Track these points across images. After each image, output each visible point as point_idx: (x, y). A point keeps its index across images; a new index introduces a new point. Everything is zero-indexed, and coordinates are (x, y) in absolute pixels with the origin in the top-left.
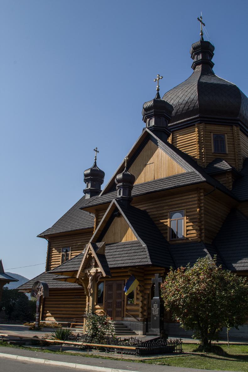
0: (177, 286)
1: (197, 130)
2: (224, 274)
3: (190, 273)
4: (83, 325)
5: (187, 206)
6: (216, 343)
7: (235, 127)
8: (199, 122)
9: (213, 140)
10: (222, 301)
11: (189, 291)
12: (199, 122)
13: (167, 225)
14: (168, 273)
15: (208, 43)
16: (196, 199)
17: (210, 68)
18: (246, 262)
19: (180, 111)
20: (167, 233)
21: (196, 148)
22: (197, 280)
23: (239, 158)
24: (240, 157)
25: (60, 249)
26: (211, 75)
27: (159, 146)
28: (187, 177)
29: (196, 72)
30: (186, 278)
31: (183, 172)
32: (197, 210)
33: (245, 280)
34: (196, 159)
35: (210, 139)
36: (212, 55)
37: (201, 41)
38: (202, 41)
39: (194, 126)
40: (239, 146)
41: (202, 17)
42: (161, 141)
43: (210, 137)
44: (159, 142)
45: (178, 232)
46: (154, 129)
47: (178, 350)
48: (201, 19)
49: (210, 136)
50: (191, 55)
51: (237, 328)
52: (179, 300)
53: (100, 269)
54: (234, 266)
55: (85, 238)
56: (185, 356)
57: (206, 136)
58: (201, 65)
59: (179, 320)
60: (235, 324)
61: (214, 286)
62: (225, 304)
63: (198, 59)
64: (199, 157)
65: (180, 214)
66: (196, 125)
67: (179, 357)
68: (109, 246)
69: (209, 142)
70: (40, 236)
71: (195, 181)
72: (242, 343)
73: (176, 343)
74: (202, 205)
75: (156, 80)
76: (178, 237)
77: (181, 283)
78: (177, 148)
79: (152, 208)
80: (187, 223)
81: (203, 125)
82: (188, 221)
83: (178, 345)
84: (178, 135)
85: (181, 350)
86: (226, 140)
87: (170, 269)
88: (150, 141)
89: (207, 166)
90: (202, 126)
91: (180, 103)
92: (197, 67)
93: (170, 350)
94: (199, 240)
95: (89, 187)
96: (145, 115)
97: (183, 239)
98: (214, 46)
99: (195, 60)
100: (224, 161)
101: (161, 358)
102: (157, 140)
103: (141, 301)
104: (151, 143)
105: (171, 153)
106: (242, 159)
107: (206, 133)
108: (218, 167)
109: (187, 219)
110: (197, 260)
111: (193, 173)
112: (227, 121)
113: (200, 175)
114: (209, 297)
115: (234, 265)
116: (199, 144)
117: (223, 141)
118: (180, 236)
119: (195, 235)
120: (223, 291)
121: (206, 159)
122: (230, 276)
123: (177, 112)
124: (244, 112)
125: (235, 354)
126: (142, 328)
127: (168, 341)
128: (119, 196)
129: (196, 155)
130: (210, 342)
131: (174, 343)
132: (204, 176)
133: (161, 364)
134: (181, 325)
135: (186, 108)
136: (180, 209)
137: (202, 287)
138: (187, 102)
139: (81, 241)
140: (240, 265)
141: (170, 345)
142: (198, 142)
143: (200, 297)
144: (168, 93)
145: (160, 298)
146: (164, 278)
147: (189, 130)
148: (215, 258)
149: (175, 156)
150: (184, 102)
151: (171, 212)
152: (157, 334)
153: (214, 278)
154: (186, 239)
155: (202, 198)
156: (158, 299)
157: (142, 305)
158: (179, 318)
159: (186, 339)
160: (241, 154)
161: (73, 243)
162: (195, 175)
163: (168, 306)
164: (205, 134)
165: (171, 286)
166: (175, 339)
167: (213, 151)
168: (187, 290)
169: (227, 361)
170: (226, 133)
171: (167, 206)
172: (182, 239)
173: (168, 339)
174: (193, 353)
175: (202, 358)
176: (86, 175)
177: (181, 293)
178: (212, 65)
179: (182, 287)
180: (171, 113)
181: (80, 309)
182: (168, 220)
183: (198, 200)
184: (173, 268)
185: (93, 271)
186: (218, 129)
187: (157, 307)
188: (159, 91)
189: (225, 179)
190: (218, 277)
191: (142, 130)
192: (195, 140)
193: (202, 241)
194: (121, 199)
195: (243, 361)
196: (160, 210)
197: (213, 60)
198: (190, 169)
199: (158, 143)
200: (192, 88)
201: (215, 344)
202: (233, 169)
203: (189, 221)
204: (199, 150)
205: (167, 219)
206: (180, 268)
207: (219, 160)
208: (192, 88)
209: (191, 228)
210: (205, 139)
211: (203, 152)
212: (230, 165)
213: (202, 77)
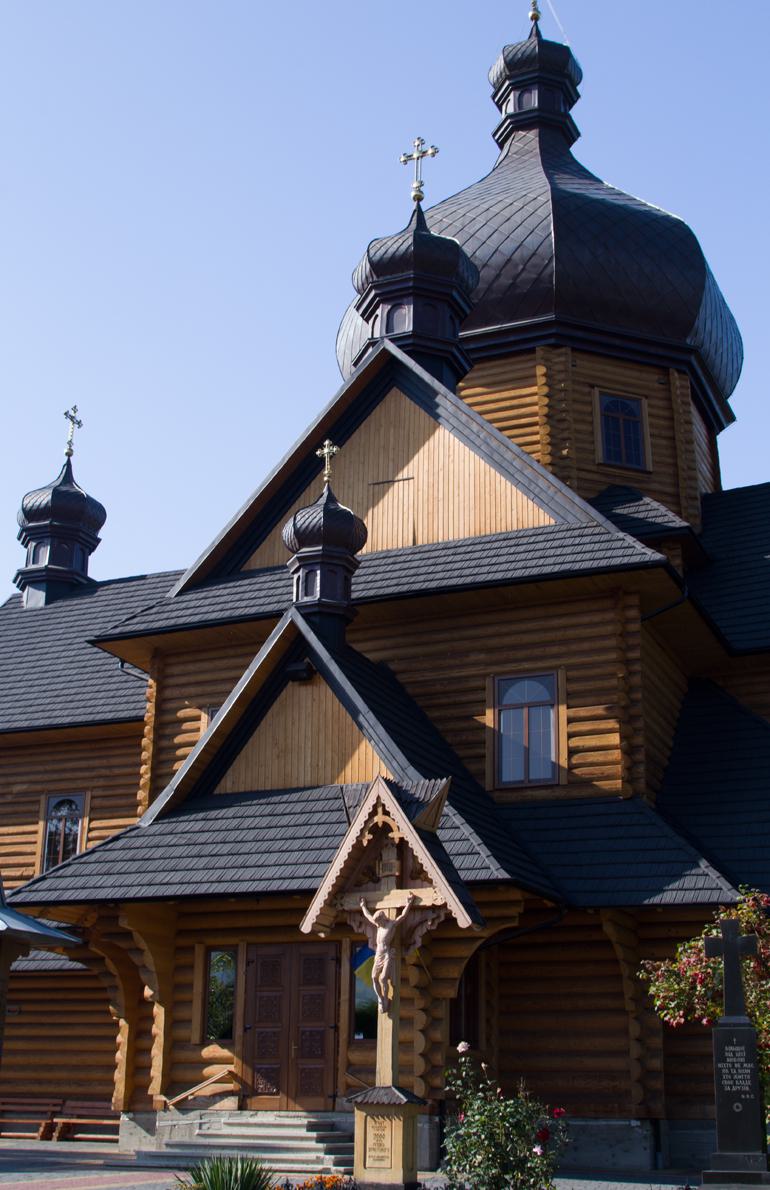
4: (117, 1126)
7: (676, 375)
8: (552, 341)
9: (602, 415)
12: (552, 341)
20: (484, 756)
35: (589, 409)
36: (572, 98)
43: (590, 403)
49: (587, 399)
50: (493, 90)
53: (438, 893)
55: (48, 768)
63: (526, 108)
66: (539, 353)
69: (583, 421)
88: (395, 391)
95: (44, 560)
102: (436, 393)
103: (422, 1031)
107: (577, 387)
112: (653, 350)
116: (551, 426)
117: (634, 426)
128: (306, 599)
135: (505, 281)
138: (509, 260)
142: (545, 419)
150: (498, 259)
157: (426, 1047)
167: (600, 456)
171: (481, 650)
176: (30, 514)
178: (571, 134)
181: (91, 1060)
183: (621, 635)
185: (395, 900)
187: (742, 1060)
188: (421, 203)
192: (536, 408)
194: (316, 609)
196: (451, 667)
199: (437, 405)
204: (550, 448)
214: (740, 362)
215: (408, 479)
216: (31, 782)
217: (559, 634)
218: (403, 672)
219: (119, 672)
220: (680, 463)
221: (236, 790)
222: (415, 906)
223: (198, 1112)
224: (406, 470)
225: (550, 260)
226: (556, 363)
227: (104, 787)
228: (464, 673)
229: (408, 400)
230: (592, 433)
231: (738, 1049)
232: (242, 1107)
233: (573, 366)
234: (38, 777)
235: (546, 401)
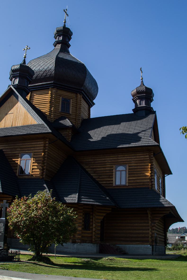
0: (20, 211)
1: (51, 92)
2: (57, 204)
3: (31, 202)
5: (35, 150)
6: (46, 255)
7: (79, 95)
8: (53, 87)
9: (62, 102)
10: (53, 225)
11: (29, 215)
12: (53, 87)
13: (18, 163)
14: (14, 200)
15: (69, 29)
16: (42, 145)
17: (67, 48)
18: (74, 197)
19: (39, 76)
20: (17, 169)
21: (47, 106)
22: (35, 207)
23: (79, 118)
24: (79, 117)
26: (67, 53)
27: (19, 101)
28: (33, 129)
29: (56, 49)
30: (27, 205)
31: (35, 124)
32: (42, 154)
33: (72, 210)
34: (47, 115)
36: (70, 39)
37: (63, 27)
38: (64, 27)
39: (48, 90)
40: (80, 109)
41: (67, 10)
42: (21, 97)
44: (19, 98)
45: (26, 169)
46: (17, 87)
47: (17, 259)
48: (66, 11)
51: (62, 244)
52: (21, 221)
54: (65, 199)
56: (21, 263)
57: (57, 98)
58: (61, 45)
59: (19, 236)
60: (61, 242)
61: (49, 213)
62: (55, 227)
63: (59, 40)
64: (49, 113)
65: (29, 156)
66: (50, 89)
67: (17, 264)
69: (57, 103)
71: (43, 132)
72: (65, 256)
73: (16, 254)
74: (47, 150)
75: (25, 49)
76: (25, 173)
77: (23, 209)
78: (33, 104)
79: (8, 149)
80: (33, 163)
81: (55, 89)
82: (34, 161)
83: (17, 255)
84: (35, 94)
85: (19, 259)
86: (71, 104)
87: (16, 198)
88: (13, 96)
89: (54, 121)
90: (54, 90)
91: (40, 70)
92: (57, 45)
93: (10, 259)
94: (41, 177)
96: (12, 75)
97: (29, 175)
98: (73, 32)
99: (57, 40)
100: (67, 119)
101: (3, 264)
102: (18, 96)
104: (13, 98)
105: (28, 107)
106: (81, 119)
107: (57, 96)
108: (62, 123)
109: (33, 160)
110: (37, 192)
111: (42, 125)
113: (48, 128)
114: (44, 221)
115: (65, 198)
118: (27, 173)
119: (38, 173)
120: (54, 217)
121: (54, 115)
122: (61, 207)
123: (37, 77)
124: (87, 85)
125: (59, 263)
126: (5, 217)
127: (9, 252)
129: (47, 112)
130: (42, 254)
131: (14, 253)
132: (50, 129)
133: (2, 269)
134: (21, 240)
135: (45, 74)
136: (29, 151)
137: (39, 213)
138: (46, 70)
140: (69, 198)
141: (11, 255)
142: (49, 102)
143: (37, 220)
144: (32, 61)
145: (6, 219)
146: (10, 204)
147: (44, 92)
148: (51, 192)
149: (30, 110)
150: (44, 70)
151: (22, 153)
152: (1, 246)
153: (49, 207)
154: (31, 175)
155: (47, 145)
156: (4, 220)
158: (19, 235)
159: (24, 251)
160: (80, 116)
162: (44, 127)
163: (12, 225)
164: (56, 97)
165: (15, 211)
166: (15, 251)
167: (60, 110)
168: (27, 214)
169: (53, 268)
170: (72, 98)
172: (28, 175)
173: (9, 250)
174: (27, 262)
175: (34, 265)
177: (23, 216)
178: (69, 46)
179: (24, 212)
180: (32, 76)
182: (19, 159)
183: (44, 146)
184: (18, 197)
187: (3, 226)
188: (25, 59)
189: (66, 133)
190: (52, 207)
191: (8, 86)
192: (48, 100)
193: (43, 178)
195: (64, 269)
196: (14, 151)
197: (94, 101)
198: (41, 122)
199: (19, 98)
200: (51, 60)
201: (45, 255)
202: (73, 126)
203: (35, 162)
204: (49, 108)
205: (18, 158)
206: (23, 198)
207: (64, 118)
208: (51, 60)
209: (36, 167)
210: (55, 101)
211: (52, 110)
212: (72, 123)
213: (60, 54)
214: (97, 93)
218: (5, 152)
220: (77, 112)
224: (9, 112)
225: (53, 71)
226: (53, 91)
228: (16, 152)
229: (15, 97)
230: (59, 106)
231: (2, 224)
233: (57, 92)
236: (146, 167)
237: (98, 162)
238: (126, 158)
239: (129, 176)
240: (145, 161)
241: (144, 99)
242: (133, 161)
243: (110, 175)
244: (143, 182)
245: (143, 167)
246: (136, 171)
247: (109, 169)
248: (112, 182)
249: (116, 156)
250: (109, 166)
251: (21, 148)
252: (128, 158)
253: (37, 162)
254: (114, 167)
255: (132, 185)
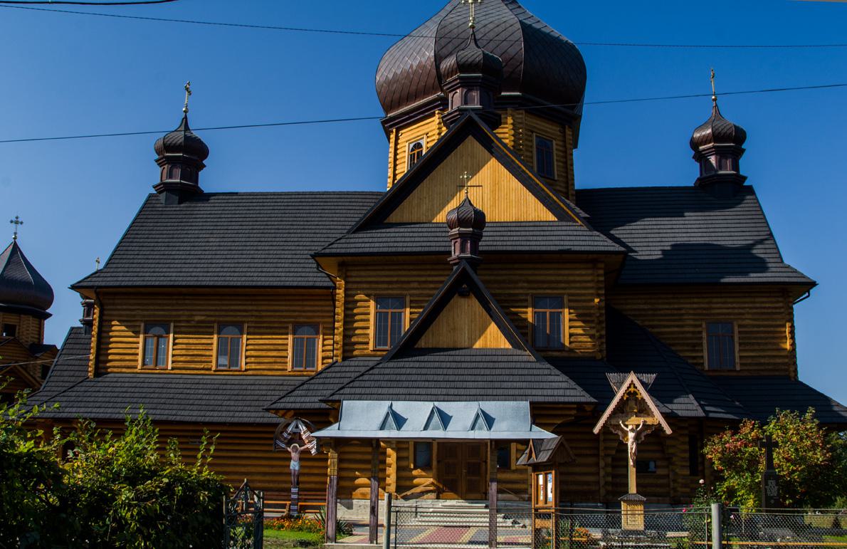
1: (512, 121)
13: (526, 319)
25: (137, 324)
66: (509, 111)
68: (446, 353)
70: (74, 287)
109: (570, 313)
139: (208, 313)
161: (179, 316)
171: (524, 282)
186: (542, 128)
203: (575, 318)
205: (527, 307)
209: (580, 331)
215: (479, 186)
216: (208, 316)
217: (565, 278)
219: (315, 270)
221: (427, 346)
222: (646, 426)
223: (414, 500)
225: (521, 63)
227: (256, 322)
228: (517, 291)
230: (532, 157)
232: (438, 498)
234: (212, 313)
235: (513, 138)
236: (779, 329)
237: (662, 312)
238: (730, 305)
239: (741, 348)
240: (775, 316)
241: (478, 88)
242: (748, 313)
243: (694, 345)
244: (775, 364)
245: (772, 329)
246: (755, 338)
247: (691, 329)
248: (702, 361)
249: (707, 300)
250: (692, 322)
251: (528, 282)
252: (734, 305)
253: (583, 318)
254: (704, 325)
255: (748, 370)
